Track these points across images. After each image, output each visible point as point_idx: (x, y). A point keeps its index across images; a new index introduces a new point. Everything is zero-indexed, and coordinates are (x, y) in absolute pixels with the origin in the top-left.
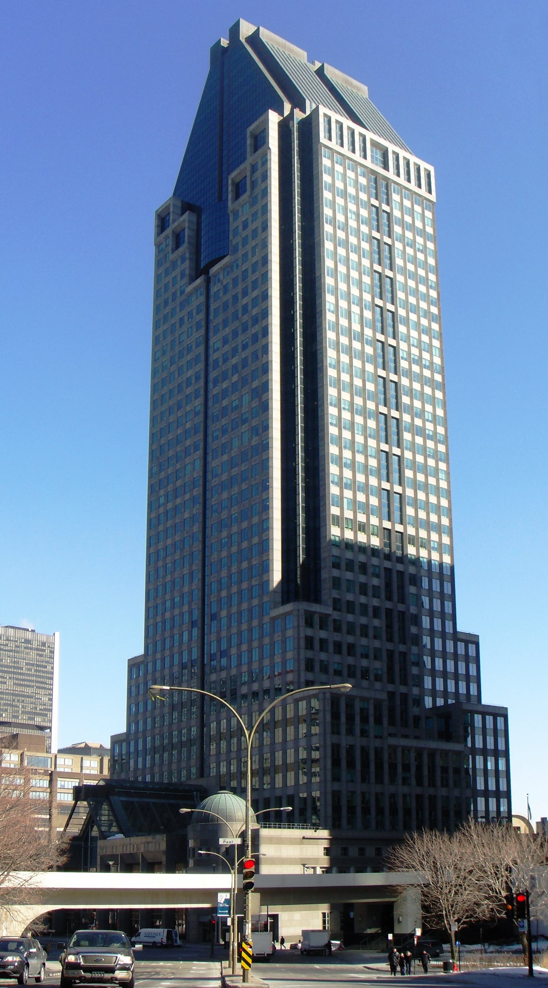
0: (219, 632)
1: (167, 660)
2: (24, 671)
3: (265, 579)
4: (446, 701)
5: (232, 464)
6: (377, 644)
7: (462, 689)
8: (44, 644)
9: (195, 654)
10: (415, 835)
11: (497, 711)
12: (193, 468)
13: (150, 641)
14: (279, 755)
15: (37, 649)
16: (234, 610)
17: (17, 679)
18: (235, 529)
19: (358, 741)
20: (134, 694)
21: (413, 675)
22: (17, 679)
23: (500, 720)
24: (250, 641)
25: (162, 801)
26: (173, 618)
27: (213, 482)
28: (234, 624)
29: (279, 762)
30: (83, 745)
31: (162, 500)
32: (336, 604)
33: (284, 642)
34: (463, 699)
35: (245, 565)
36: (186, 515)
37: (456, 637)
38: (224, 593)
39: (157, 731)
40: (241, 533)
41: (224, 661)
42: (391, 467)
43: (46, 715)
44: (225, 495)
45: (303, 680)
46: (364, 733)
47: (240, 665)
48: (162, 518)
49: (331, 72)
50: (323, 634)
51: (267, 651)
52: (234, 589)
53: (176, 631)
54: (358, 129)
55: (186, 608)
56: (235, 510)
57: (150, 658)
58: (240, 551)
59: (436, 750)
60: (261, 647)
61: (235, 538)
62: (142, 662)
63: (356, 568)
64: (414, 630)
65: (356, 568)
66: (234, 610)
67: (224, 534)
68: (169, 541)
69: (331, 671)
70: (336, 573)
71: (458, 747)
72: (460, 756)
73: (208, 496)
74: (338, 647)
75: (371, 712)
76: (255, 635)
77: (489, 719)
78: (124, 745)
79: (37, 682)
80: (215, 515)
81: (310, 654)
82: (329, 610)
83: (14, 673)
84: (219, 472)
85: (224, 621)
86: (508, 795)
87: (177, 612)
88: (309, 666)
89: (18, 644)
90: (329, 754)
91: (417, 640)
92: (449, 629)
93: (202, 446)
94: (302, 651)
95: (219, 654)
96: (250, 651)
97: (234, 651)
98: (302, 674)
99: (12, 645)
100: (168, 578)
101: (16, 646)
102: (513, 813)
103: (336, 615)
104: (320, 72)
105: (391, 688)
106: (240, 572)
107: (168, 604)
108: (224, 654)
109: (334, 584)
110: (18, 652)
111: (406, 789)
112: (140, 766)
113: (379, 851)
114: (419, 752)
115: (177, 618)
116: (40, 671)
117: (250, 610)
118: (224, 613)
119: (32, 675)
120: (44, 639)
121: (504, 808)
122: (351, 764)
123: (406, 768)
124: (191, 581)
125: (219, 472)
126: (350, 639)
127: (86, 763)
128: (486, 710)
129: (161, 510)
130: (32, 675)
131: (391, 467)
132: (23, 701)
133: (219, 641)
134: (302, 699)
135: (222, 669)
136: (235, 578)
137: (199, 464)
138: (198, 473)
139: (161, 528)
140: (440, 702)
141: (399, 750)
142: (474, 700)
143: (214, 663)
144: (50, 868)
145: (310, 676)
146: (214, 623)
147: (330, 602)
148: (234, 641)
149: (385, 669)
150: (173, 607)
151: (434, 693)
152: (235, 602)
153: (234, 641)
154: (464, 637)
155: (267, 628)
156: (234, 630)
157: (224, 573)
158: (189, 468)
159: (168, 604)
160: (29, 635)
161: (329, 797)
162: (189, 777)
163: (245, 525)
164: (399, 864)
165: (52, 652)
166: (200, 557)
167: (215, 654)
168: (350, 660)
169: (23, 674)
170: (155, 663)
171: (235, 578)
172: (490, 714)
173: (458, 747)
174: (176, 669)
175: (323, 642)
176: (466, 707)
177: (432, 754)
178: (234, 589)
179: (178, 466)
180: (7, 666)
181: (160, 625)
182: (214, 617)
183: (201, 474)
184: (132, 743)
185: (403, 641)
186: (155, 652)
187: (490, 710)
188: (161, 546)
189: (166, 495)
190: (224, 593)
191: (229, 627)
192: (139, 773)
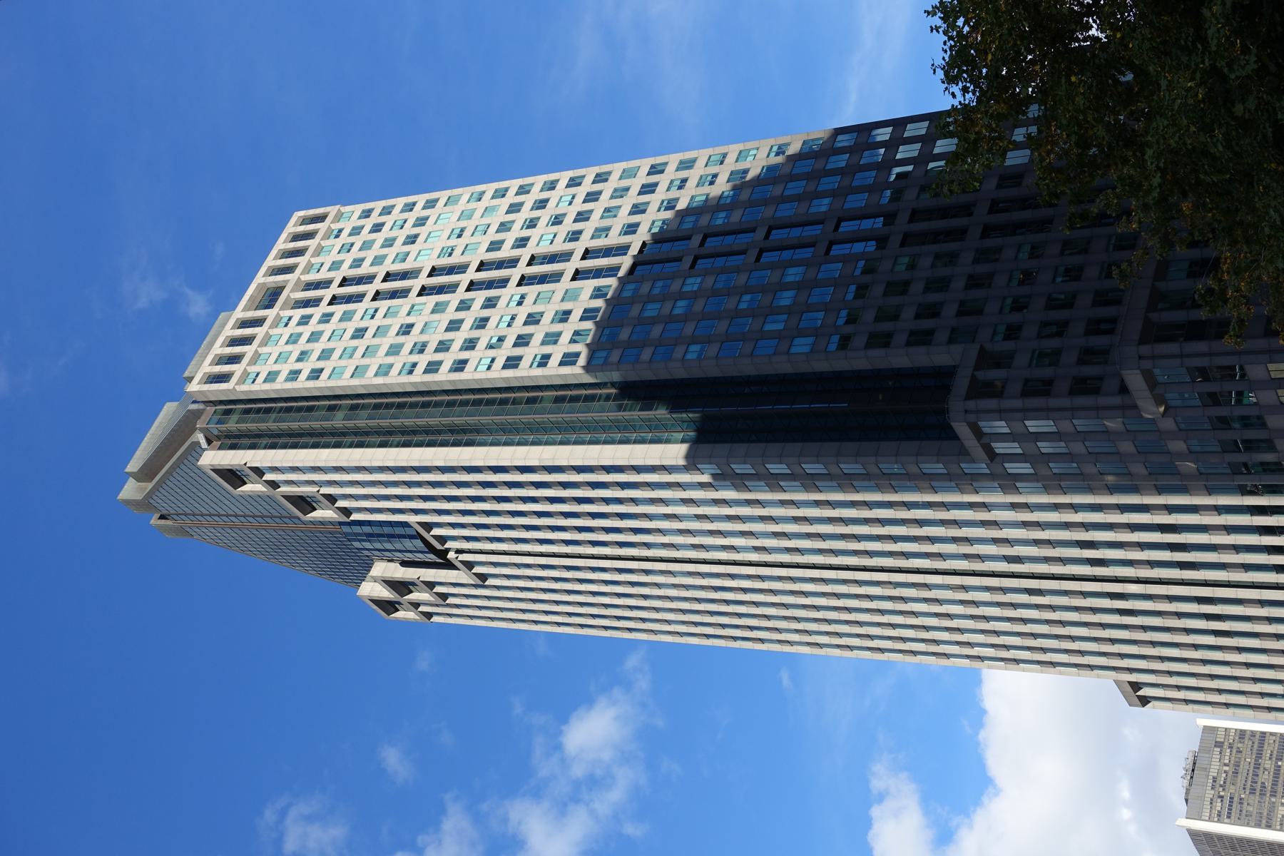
45: (1117, 400)
88: (1083, 387)
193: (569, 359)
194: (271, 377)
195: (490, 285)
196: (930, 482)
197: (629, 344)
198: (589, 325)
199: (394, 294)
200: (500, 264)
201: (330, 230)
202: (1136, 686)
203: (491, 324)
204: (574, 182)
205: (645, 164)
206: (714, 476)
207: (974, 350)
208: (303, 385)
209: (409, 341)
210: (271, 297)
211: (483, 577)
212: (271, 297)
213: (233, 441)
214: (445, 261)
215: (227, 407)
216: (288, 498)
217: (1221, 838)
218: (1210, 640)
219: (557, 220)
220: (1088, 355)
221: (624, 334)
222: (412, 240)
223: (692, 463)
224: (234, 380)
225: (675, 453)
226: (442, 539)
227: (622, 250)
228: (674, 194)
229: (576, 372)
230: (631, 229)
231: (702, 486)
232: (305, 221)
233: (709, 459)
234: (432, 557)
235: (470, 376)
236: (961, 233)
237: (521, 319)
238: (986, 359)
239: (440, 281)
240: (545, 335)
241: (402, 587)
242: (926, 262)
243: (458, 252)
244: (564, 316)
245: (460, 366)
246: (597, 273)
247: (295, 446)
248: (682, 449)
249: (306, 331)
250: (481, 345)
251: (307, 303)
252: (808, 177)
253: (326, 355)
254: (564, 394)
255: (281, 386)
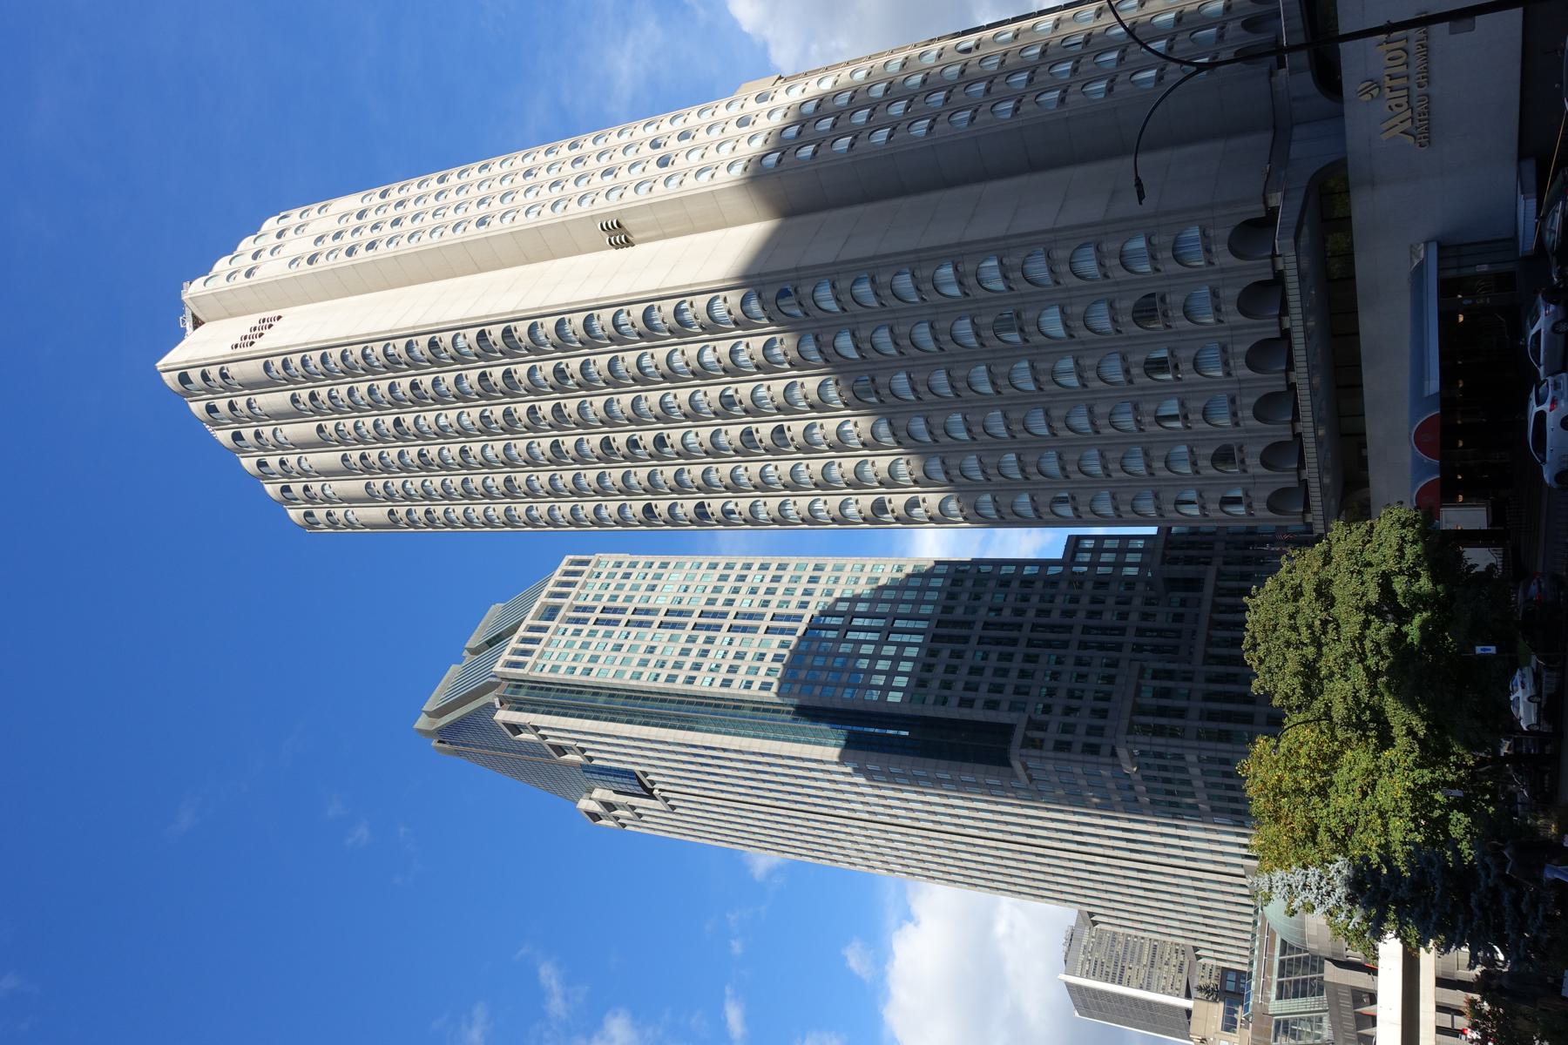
45: (1109, 760)
49: (474, 641)
54: (521, 632)
70: (954, 701)
88: (1092, 749)
104: (475, 652)
105: (974, 641)
145: (1106, 750)
193: (765, 686)
194: (555, 669)
195: (708, 627)
196: (989, 789)
197: (805, 682)
198: (778, 665)
199: (640, 624)
200: (615, 610)
201: (592, 572)
202: (1091, 914)
203: (711, 655)
204: (764, 567)
205: (812, 562)
206: (855, 769)
207: (1025, 718)
208: (577, 677)
209: (653, 659)
210: (551, 613)
211: (674, 807)
212: (551, 613)
213: (519, 706)
214: (676, 607)
215: (518, 684)
216: (551, 746)
217: (1087, 989)
218: (1141, 893)
219: (754, 591)
220: (1093, 730)
221: (802, 675)
222: (652, 588)
223: (842, 760)
224: (528, 667)
225: (832, 753)
226: (653, 783)
227: (799, 618)
228: (831, 586)
229: (770, 695)
230: (804, 605)
231: (844, 773)
232: (572, 563)
233: (853, 760)
234: (640, 790)
235: (695, 688)
236: (966, 640)
237: (731, 655)
238: (1034, 725)
239: (674, 619)
240: (753, 666)
241: (609, 806)
242: (993, 657)
243: (685, 602)
244: (761, 657)
245: (588, 672)
246: (782, 631)
247: (565, 715)
248: (837, 751)
249: (579, 641)
250: (705, 668)
251: (577, 621)
252: (917, 589)
253: (594, 659)
254: (759, 707)
255: (561, 676)
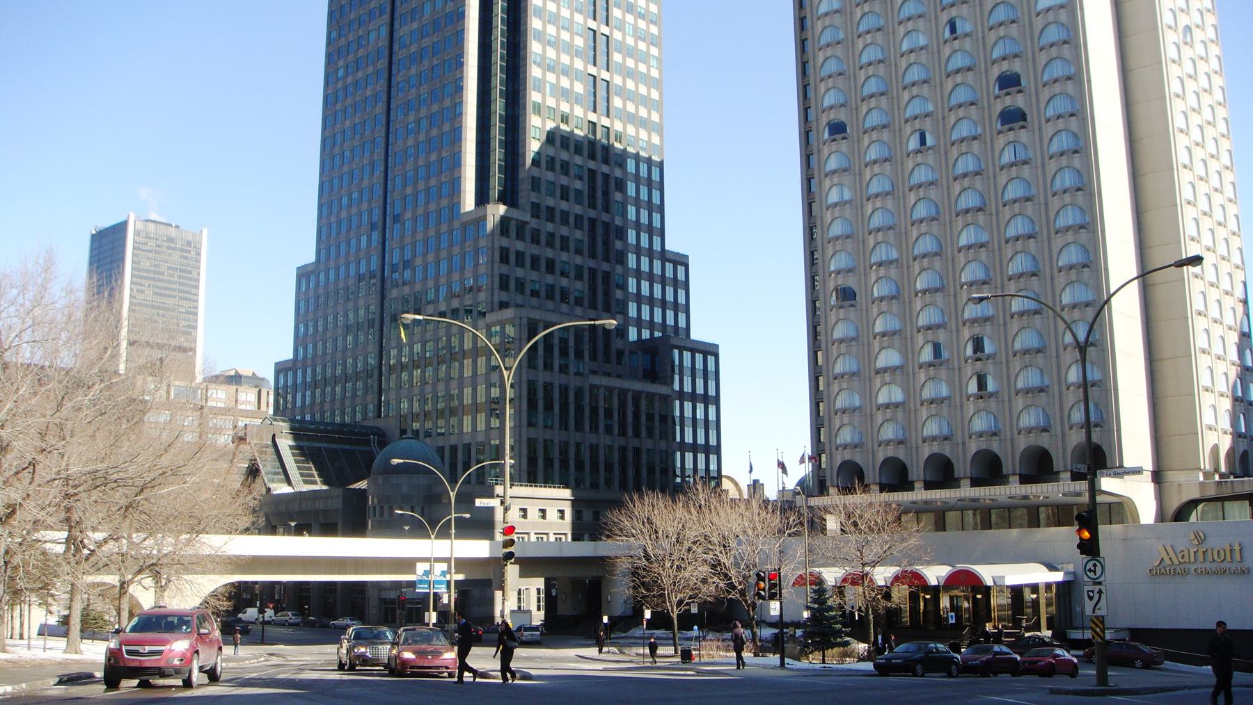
0: (402, 237)
1: (342, 269)
2: (166, 277)
3: (456, 175)
4: (652, 334)
5: (422, 33)
6: (578, 260)
7: (670, 321)
8: (189, 244)
9: (375, 264)
10: (636, 497)
11: (707, 348)
12: (377, 35)
13: (323, 246)
14: (468, 391)
15: (182, 250)
16: (420, 211)
17: (157, 287)
18: (423, 113)
19: (557, 379)
20: (302, 312)
21: (617, 300)
22: (157, 287)
23: (711, 359)
24: (438, 250)
25: (336, 446)
26: (350, 219)
27: (400, 54)
28: (420, 228)
29: (467, 400)
30: (233, 373)
31: (341, 73)
32: (536, 210)
33: (476, 252)
34: (670, 332)
35: (434, 157)
36: (369, 93)
37: (665, 256)
38: (409, 190)
39: (328, 358)
40: (431, 117)
41: (407, 274)
42: (599, 48)
43: (190, 334)
44: (413, 71)
46: (564, 369)
47: (425, 278)
48: (341, 94)
50: (520, 246)
51: (457, 261)
52: (421, 186)
53: (352, 234)
55: (364, 207)
56: (424, 89)
57: (322, 267)
58: (429, 140)
59: (640, 393)
60: (450, 259)
61: (424, 123)
62: (312, 272)
63: (558, 167)
64: (618, 245)
65: (558, 167)
66: (420, 211)
67: (412, 118)
68: (348, 123)
69: (528, 292)
71: (663, 390)
72: (666, 400)
73: (394, 72)
74: (535, 261)
75: (571, 343)
76: (444, 244)
77: (699, 357)
78: (290, 373)
79: (180, 291)
80: (401, 95)
81: (505, 269)
82: (526, 217)
83: (154, 279)
84: (408, 43)
85: (408, 224)
86: (718, 450)
87: (354, 211)
88: (504, 283)
89: (159, 243)
90: (525, 393)
91: (621, 258)
92: (657, 247)
93: (388, 9)
94: (497, 265)
95: (401, 265)
96: (438, 263)
97: (418, 261)
98: (496, 292)
99: (152, 244)
100: (346, 169)
101: (157, 246)
102: (723, 473)
103: (534, 223)
106: (428, 165)
107: (345, 201)
108: (407, 264)
109: (533, 185)
110: (159, 253)
111: (548, 435)
112: (299, 404)
113: (597, 515)
114: (623, 393)
115: (355, 219)
116: (184, 278)
117: (439, 212)
118: (408, 215)
119: (175, 283)
120: (190, 238)
121: (713, 467)
122: (549, 407)
123: (609, 413)
124: (372, 174)
125: (408, 43)
126: (550, 253)
127: (242, 397)
128: (695, 346)
129: (340, 85)
130: (175, 283)
131: (599, 48)
132: (164, 315)
133: (402, 249)
134: (495, 324)
135: (405, 284)
136: (422, 172)
137: (384, 31)
138: (383, 43)
139: (338, 107)
140: (646, 334)
141: (630, 395)
142: (682, 335)
143: (396, 275)
144: (247, 531)
145: (504, 297)
146: (397, 227)
147: (528, 207)
148: (420, 249)
149: (586, 291)
150: (350, 205)
151: (639, 323)
152: (422, 199)
153: (420, 249)
154: (672, 257)
155: (457, 234)
156: (420, 236)
157: (410, 165)
158: (373, 35)
159: (345, 201)
160: (172, 232)
161: (524, 446)
162: (365, 417)
163: (435, 108)
164: (618, 532)
165: (199, 254)
166: (383, 145)
167: (397, 264)
168: (550, 279)
169: (164, 281)
170: (327, 273)
171: (422, 172)
172: (700, 352)
173: (663, 390)
174: (351, 282)
175: (520, 255)
176: (674, 341)
177: (637, 396)
178: (421, 186)
179: (361, 33)
180: (145, 271)
181: (334, 226)
182: (396, 219)
183: (387, 43)
184: (300, 372)
185: (607, 259)
186: (328, 258)
187: (700, 347)
188: (338, 128)
189: (346, 67)
190: (409, 190)
191: (414, 231)
192: (298, 411)
